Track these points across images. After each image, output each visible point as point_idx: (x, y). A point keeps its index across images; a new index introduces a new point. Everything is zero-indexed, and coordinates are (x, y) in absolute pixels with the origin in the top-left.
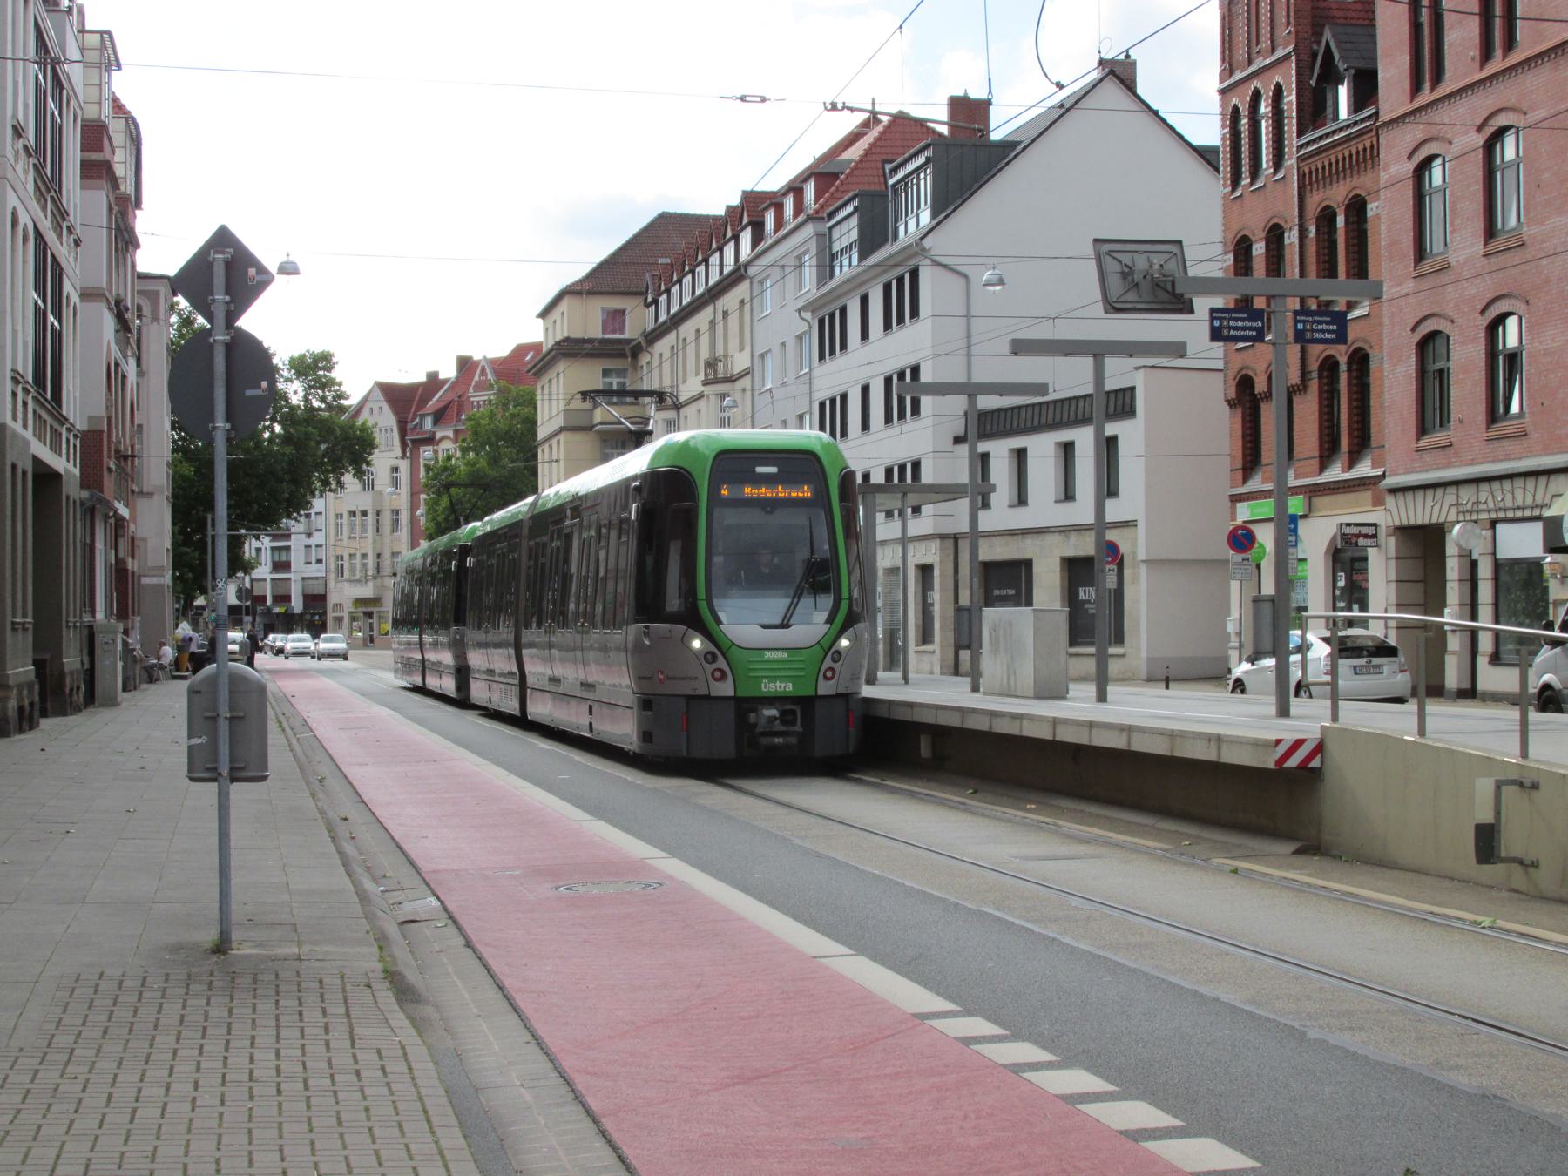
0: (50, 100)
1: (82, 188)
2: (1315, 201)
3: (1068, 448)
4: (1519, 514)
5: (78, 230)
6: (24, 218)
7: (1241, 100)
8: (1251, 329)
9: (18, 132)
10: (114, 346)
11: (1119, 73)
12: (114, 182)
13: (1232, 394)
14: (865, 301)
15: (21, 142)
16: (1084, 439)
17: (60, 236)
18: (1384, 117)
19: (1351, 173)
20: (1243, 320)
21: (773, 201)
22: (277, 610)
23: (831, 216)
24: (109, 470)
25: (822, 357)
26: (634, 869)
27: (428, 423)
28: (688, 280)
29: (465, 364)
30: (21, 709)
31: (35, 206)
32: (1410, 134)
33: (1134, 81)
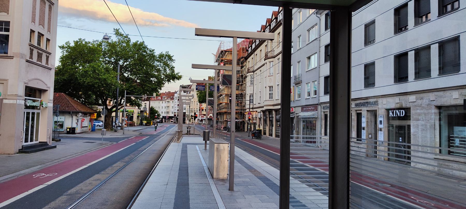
8: (203, 88)
20: (201, 87)
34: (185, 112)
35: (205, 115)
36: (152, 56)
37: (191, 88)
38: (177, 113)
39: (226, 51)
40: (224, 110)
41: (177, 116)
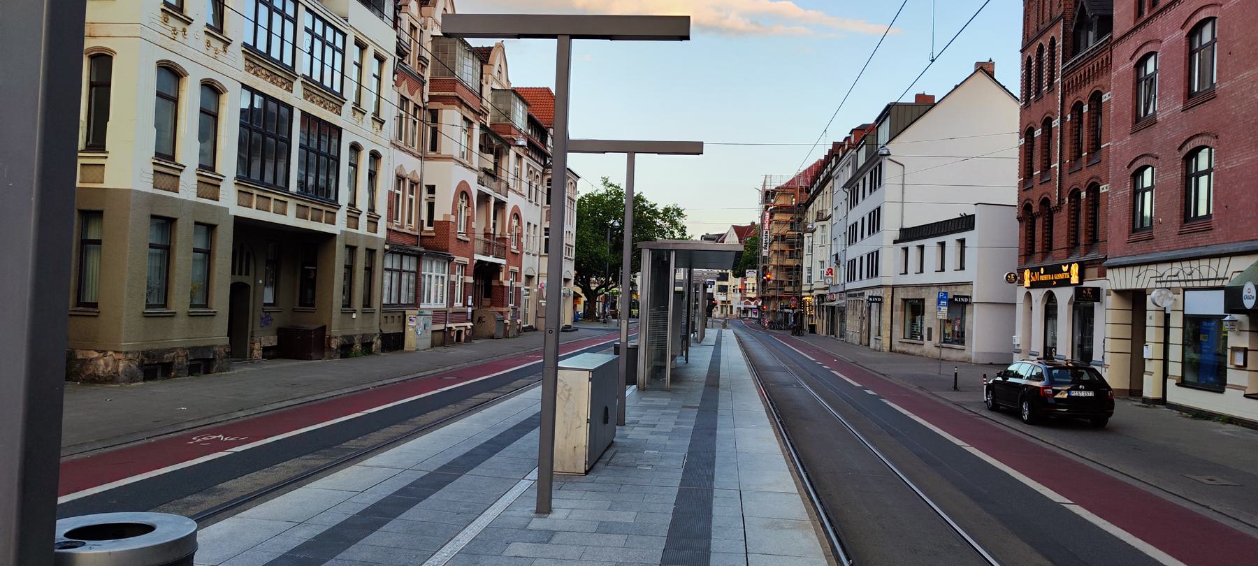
2: (1070, 101)
3: (942, 245)
7: (1033, 53)
16: (951, 240)
35: (752, 299)
36: (655, 213)
37: (725, 243)
39: (774, 191)
40: (772, 293)
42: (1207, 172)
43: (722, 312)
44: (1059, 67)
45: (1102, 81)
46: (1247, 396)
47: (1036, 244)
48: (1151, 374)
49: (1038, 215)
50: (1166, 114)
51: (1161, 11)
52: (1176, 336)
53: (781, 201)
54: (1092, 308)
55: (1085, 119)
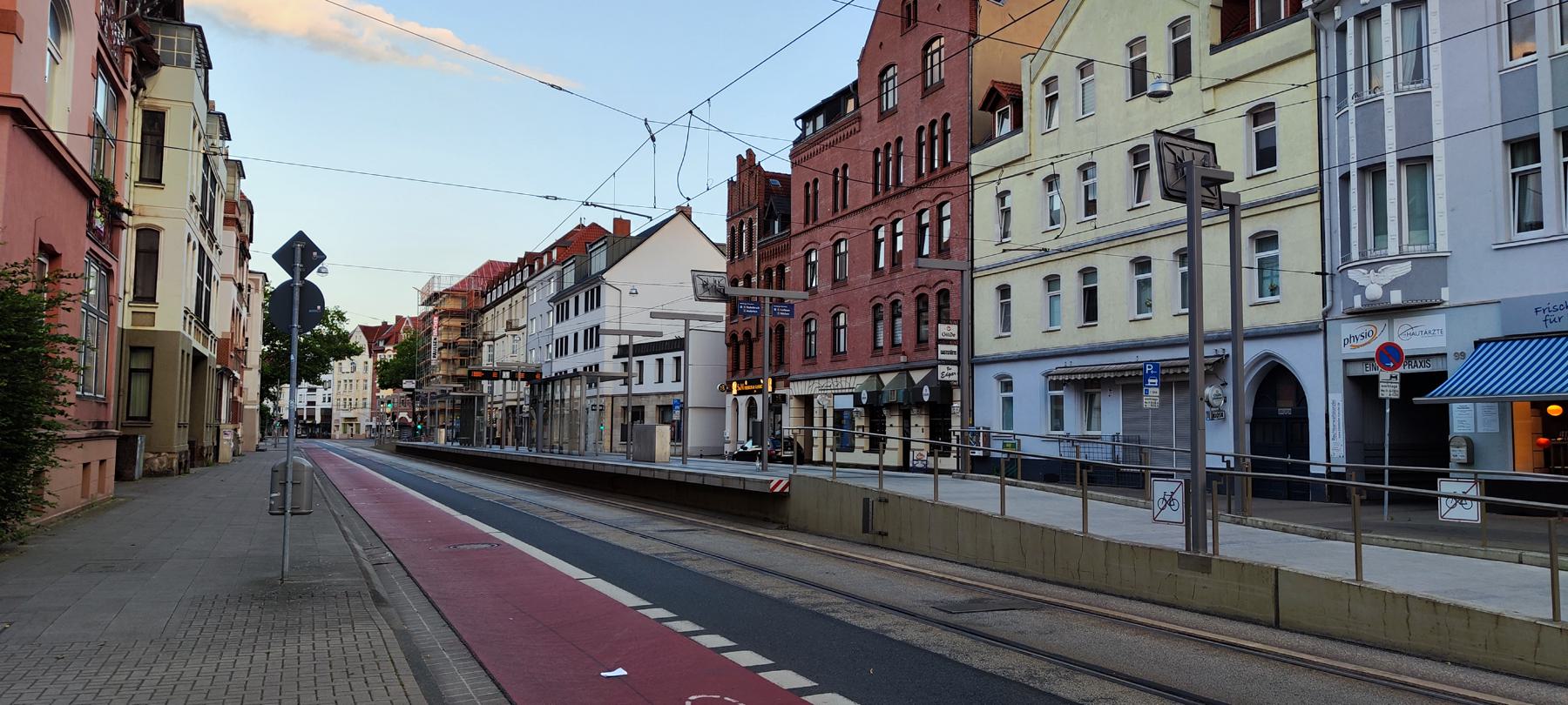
0: (209, 187)
1: (224, 229)
2: (764, 266)
3: (661, 361)
4: (843, 391)
5: (221, 247)
6: (193, 239)
7: (736, 224)
9: (193, 199)
10: (236, 301)
11: (684, 212)
12: (240, 229)
13: (728, 341)
14: (577, 298)
15: (195, 204)
16: (668, 358)
17: (212, 249)
18: (793, 232)
19: (459, 379)
21: (539, 256)
22: (308, 422)
23: (563, 264)
24: (231, 356)
25: (558, 321)
26: (487, 536)
27: (381, 344)
28: (519, 274)
29: (399, 319)
30: (180, 464)
31: (200, 235)
32: (803, 240)
33: (690, 216)
34: (330, 407)
38: (305, 411)
39: (442, 293)
41: (305, 418)
42: (844, 327)
43: (345, 432)
44: (756, 242)
45: (785, 258)
46: (864, 452)
47: (741, 363)
48: (817, 446)
49: (742, 343)
50: (823, 289)
51: (819, 226)
52: (830, 422)
53: (451, 304)
54: (781, 408)
55: (774, 281)
